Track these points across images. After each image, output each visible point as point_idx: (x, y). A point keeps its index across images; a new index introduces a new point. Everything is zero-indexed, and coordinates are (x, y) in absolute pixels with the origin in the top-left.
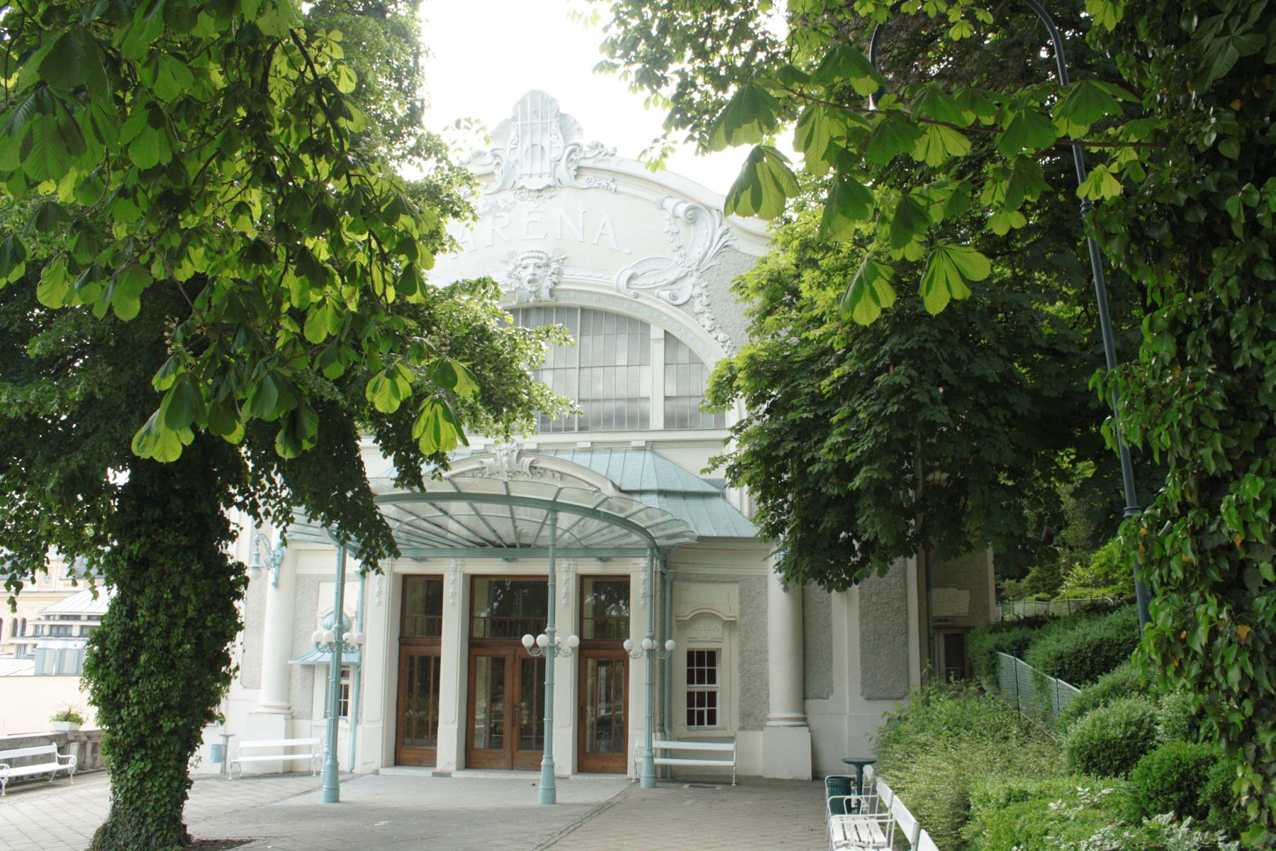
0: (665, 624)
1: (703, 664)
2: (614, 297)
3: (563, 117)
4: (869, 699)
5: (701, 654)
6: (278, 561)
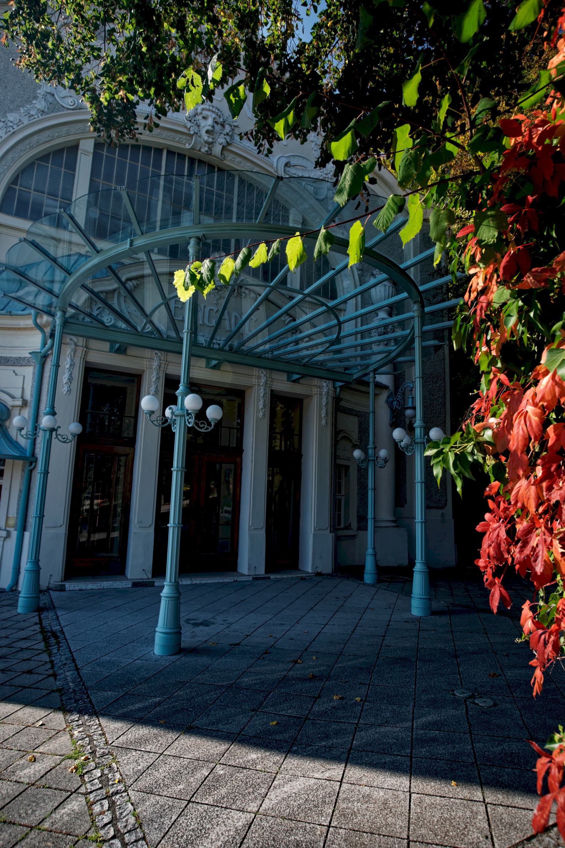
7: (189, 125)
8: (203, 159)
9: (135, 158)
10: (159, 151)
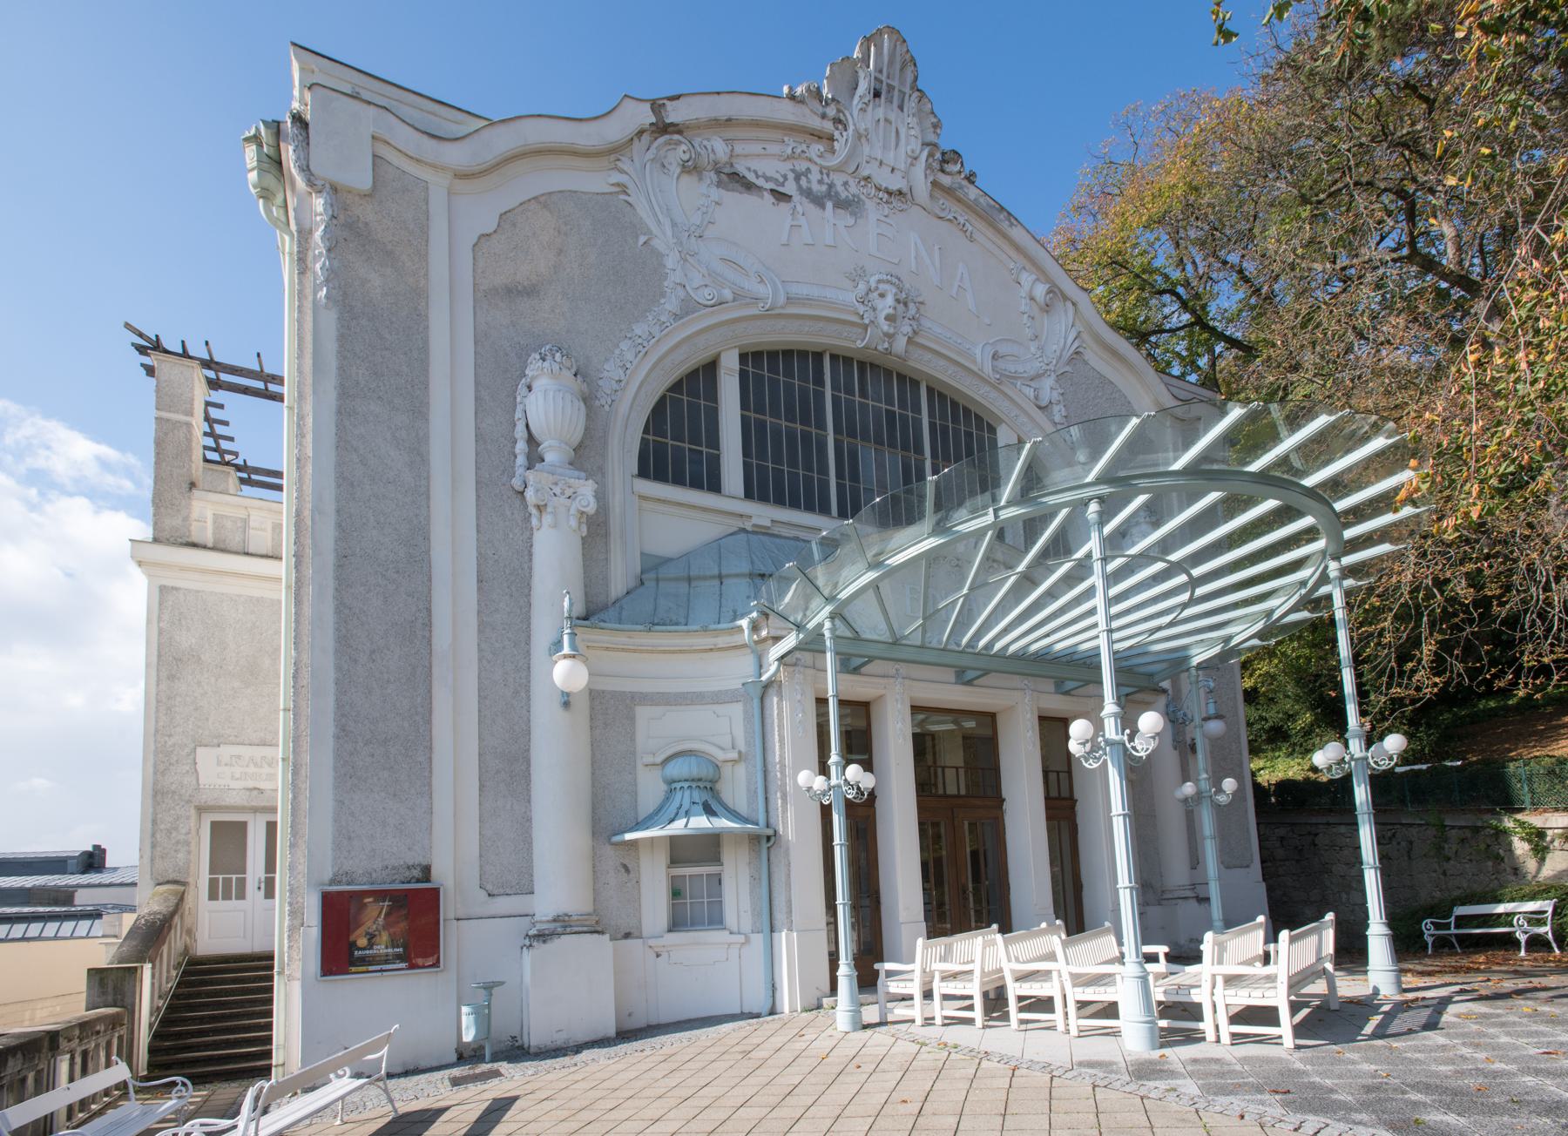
7: (861, 309)
8: (877, 362)
9: (789, 373)
10: (818, 356)
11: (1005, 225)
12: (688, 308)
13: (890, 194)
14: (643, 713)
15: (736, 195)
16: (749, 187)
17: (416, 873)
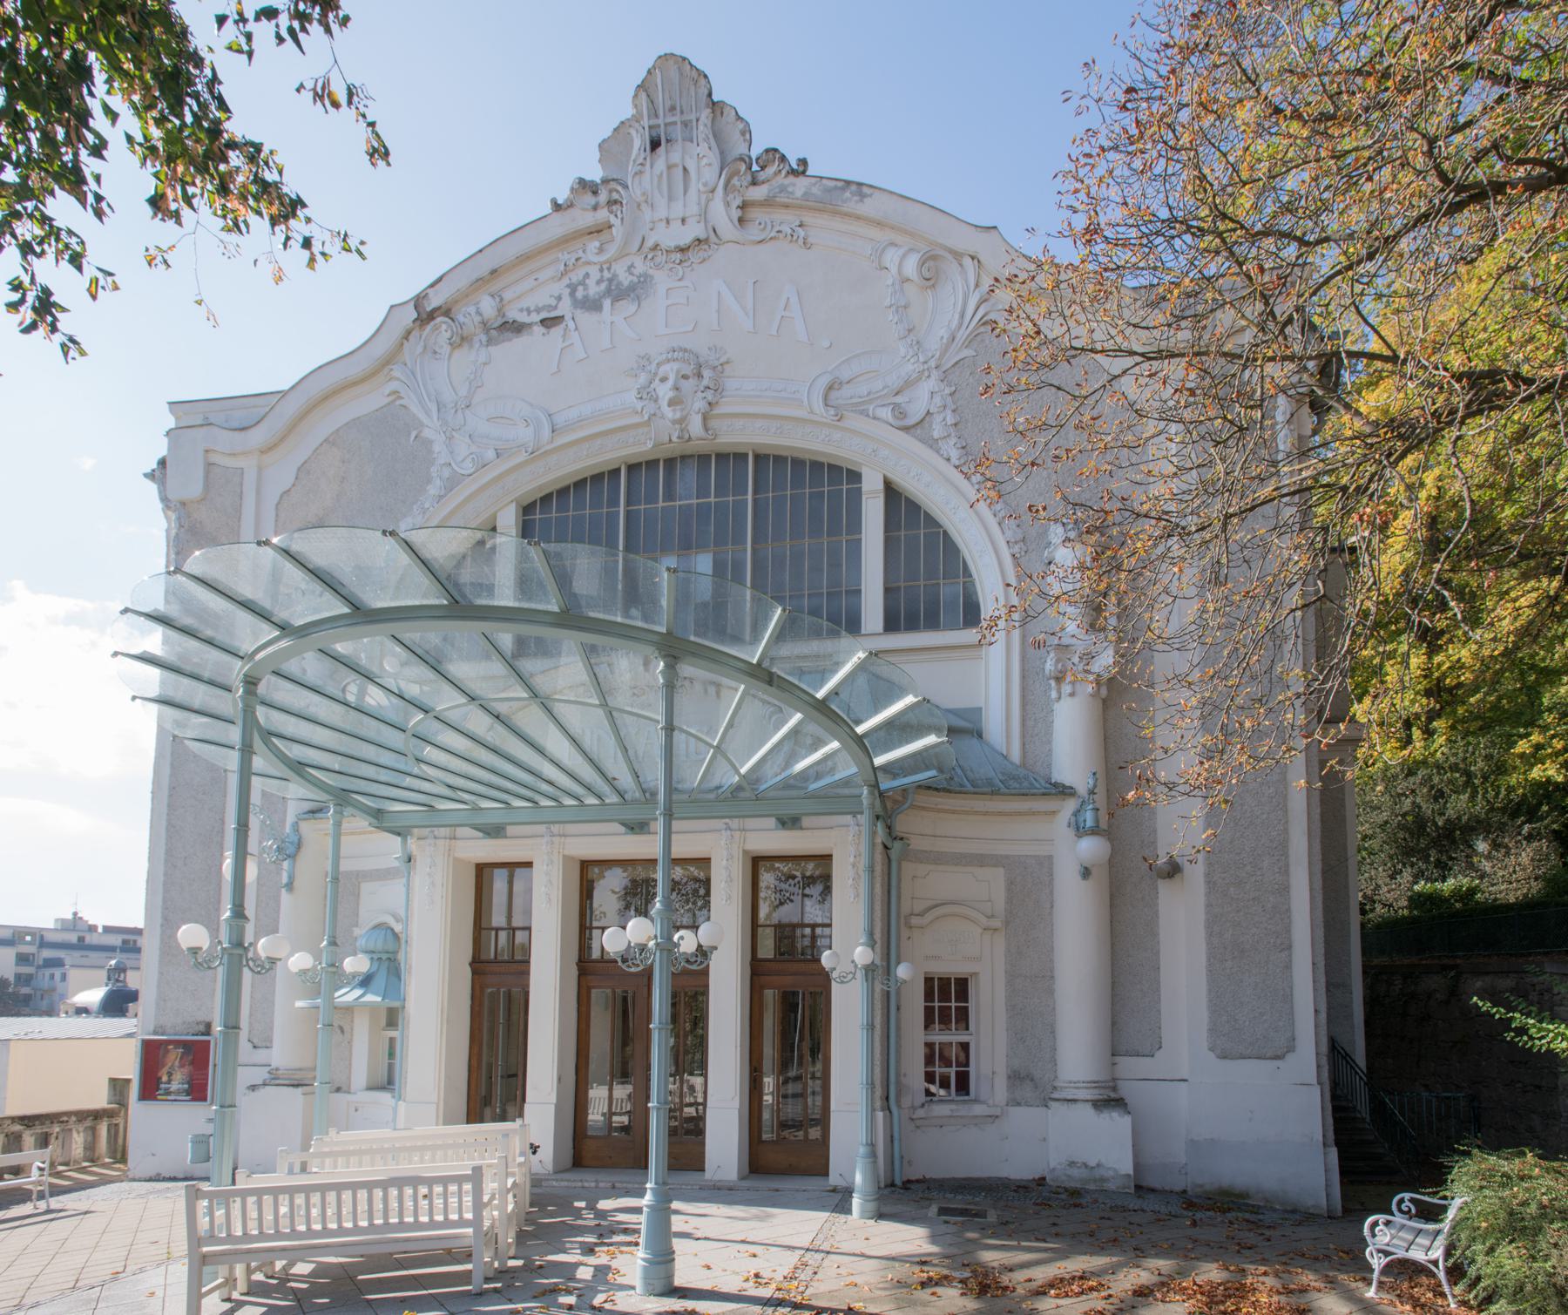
0: (890, 929)
1: (948, 998)
2: (804, 421)
3: (716, 107)
4: (1224, 1056)
5: (945, 982)
6: (291, 850)
11: (853, 206)
12: (453, 483)
13: (682, 250)
14: (366, 887)
15: (506, 345)
16: (517, 328)
17: (202, 1028)
